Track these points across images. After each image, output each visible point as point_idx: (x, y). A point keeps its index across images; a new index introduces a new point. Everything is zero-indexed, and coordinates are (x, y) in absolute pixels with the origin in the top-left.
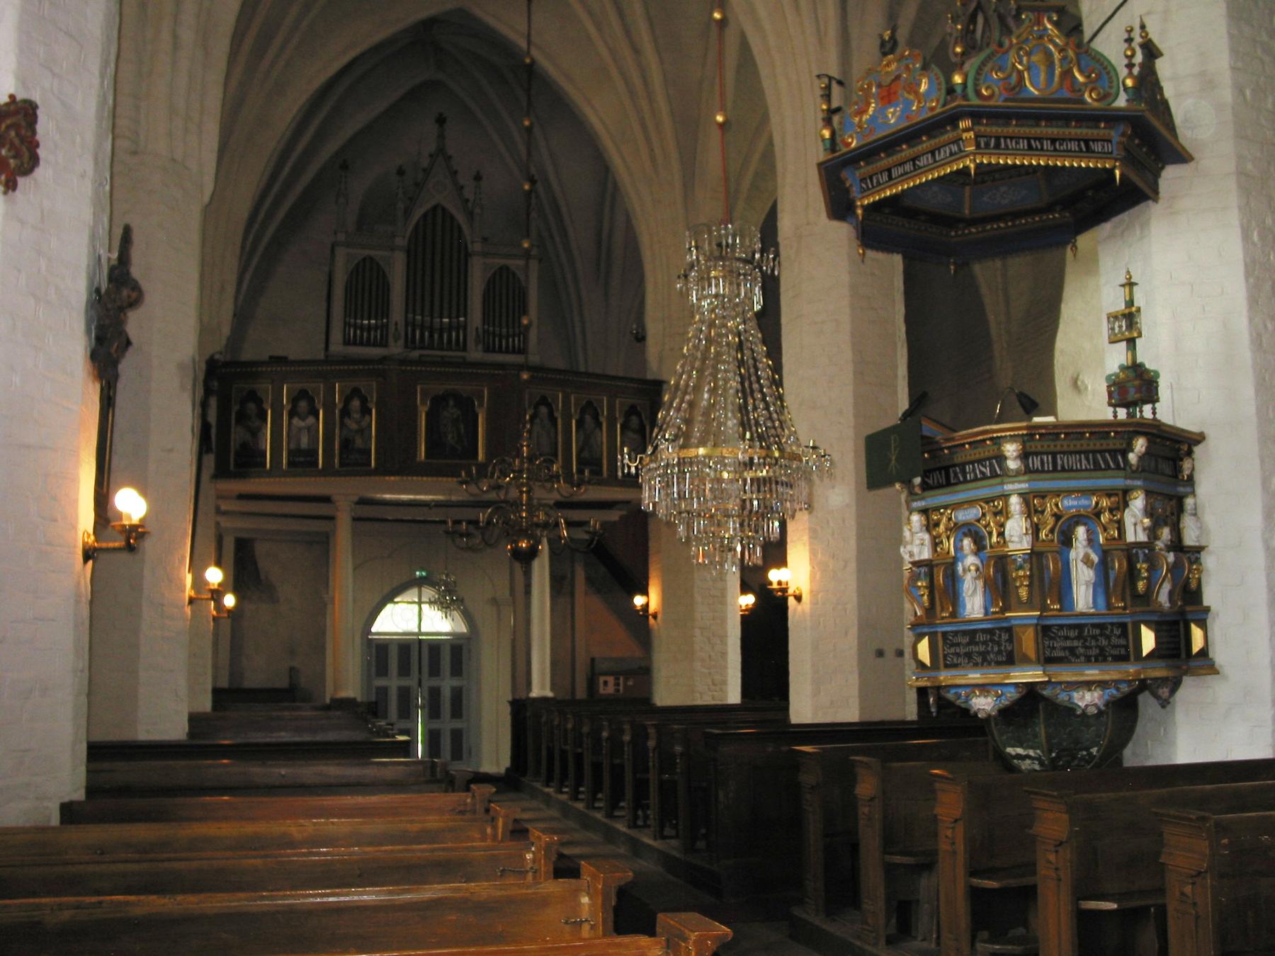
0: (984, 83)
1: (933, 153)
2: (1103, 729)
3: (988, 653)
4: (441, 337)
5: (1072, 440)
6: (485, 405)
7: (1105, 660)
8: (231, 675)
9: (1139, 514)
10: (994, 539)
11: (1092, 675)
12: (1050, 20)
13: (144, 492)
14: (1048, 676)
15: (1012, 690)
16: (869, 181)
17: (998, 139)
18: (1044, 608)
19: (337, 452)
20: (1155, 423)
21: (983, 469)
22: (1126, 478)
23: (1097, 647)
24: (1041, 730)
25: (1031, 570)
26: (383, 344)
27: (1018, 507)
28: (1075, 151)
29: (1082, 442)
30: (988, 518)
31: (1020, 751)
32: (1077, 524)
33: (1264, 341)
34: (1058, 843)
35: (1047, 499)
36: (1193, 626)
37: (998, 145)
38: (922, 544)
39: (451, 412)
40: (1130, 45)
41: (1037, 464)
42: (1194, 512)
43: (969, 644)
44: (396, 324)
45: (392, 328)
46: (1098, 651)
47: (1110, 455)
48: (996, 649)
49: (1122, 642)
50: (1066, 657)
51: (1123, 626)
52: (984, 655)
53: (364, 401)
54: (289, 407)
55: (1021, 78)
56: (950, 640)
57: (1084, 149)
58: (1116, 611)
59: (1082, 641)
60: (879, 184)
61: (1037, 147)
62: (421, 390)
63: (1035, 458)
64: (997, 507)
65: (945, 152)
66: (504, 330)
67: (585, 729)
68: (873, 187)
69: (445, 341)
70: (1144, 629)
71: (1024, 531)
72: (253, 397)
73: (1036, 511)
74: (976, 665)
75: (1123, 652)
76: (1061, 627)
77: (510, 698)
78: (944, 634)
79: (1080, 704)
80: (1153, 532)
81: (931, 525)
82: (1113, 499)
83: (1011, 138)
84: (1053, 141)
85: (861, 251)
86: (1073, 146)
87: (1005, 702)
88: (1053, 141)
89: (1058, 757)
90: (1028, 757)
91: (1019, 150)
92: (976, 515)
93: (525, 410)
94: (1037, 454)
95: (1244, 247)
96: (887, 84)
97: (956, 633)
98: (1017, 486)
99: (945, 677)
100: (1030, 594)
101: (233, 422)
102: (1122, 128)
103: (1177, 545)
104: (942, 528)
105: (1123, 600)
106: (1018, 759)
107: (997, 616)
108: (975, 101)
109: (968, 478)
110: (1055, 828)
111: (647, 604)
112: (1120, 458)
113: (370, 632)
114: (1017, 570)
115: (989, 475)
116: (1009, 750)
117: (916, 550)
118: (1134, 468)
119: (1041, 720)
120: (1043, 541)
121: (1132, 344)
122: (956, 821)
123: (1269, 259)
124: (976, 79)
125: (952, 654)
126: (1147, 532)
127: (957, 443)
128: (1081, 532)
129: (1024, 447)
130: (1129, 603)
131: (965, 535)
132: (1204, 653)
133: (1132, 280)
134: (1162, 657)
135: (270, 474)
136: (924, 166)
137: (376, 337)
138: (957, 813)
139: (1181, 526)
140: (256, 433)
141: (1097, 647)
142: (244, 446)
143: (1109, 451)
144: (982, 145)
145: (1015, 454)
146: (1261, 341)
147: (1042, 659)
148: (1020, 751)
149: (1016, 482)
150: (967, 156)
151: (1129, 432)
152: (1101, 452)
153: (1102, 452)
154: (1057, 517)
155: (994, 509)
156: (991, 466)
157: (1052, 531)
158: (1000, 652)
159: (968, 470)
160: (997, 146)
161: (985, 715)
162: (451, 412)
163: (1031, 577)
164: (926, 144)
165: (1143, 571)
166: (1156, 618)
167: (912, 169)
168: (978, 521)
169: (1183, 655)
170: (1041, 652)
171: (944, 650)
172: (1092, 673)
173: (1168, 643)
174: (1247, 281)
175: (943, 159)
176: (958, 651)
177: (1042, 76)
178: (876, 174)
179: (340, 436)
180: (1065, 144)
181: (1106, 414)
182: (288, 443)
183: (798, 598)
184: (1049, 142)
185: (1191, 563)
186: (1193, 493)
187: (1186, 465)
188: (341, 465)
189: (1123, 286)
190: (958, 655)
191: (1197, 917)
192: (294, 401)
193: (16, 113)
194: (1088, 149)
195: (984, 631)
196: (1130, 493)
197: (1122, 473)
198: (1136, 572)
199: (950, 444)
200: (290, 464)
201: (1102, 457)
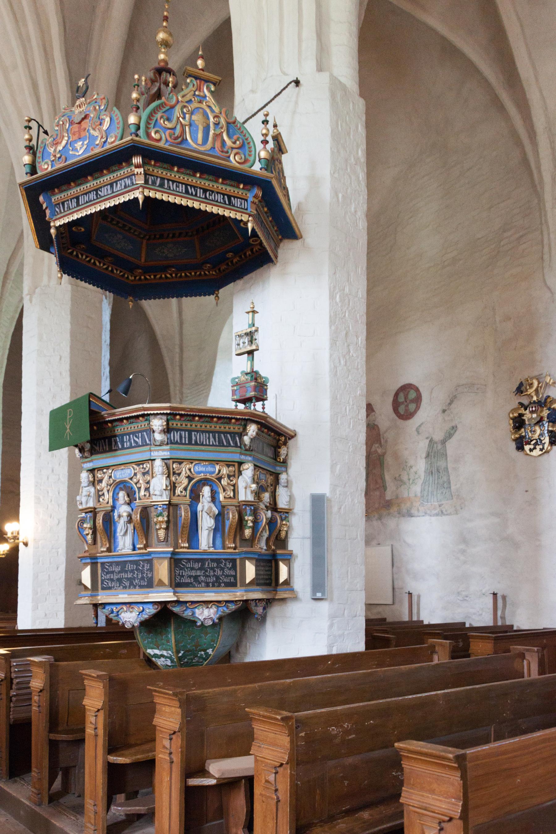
0: (154, 128)
1: (111, 185)
2: (216, 636)
5: (203, 422)
7: (219, 586)
9: (249, 481)
10: (142, 493)
11: (123, 598)
12: (208, 88)
14: (177, 596)
16: (61, 205)
18: (176, 546)
20: (263, 414)
21: (137, 440)
22: (241, 454)
24: (172, 636)
25: (168, 516)
27: (161, 469)
28: (220, 203)
29: (211, 424)
30: (138, 477)
31: (157, 652)
32: (204, 485)
34: (172, 732)
35: (183, 465)
38: (89, 496)
40: (265, 146)
41: (177, 437)
42: (286, 484)
47: (231, 436)
48: (140, 576)
50: (191, 583)
52: (131, 580)
55: (183, 132)
56: (107, 569)
57: (227, 203)
59: (203, 571)
60: (69, 208)
61: (192, 193)
63: (175, 433)
64: (145, 469)
65: (121, 185)
68: (64, 211)
70: (247, 563)
71: (164, 487)
73: (174, 473)
74: (125, 587)
75: (232, 580)
76: (189, 560)
78: (103, 564)
79: (200, 618)
80: (258, 494)
81: (96, 482)
82: (230, 468)
83: (173, 182)
84: (205, 191)
85: (59, 275)
86: (219, 198)
87: (145, 616)
88: (205, 191)
89: (184, 656)
90: (162, 656)
92: (130, 474)
94: (177, 430)
96: (77, 122)
97: (111, 563)
98: (161, 453)
99: (103, 597)
100: (167, 535)
103: (273, 507)
104: (104, 484)
105: (234, 542)
106: (155, 658)
107: (141, 551)
108: (143, 139)
109: (125, 446)
110: (171, 720)
112: (237, 439)
114: (158, 516)
115: (140, 444)
116: (149, 651)
117: (84, 500)
118: (247, 447)
119: (172, 629)
120: (179, 496)
121: (251, 356)
122: (98, 710)
123: (345, 316)
124: (148, 123)
125: (108, 579)
126: (254, 494)
127: (116, 418)
128: (206, 491)
129: (168, 424)
130: (238, 545)
131: (121, 489)
132: (287, 582)
133: (255, 309)
136: (105, 196)
138: (99, 704)
139: (277, 494)
143: (230, 433)
144: (150, 182)
145: (161, 428)
146: (336, 371)
147: (174, 584)
148: (157, 652)
149: (160, 450)
150: (138, 188)
151: (245, 419)
153: (225, 433)
154: (190, 479)
155: (142, 470)
156: (143, 437)
157: (185, 489)
158: (142, 578)
159: (125, 440)
160: (162, 185)
161: (130, 626)
163: (168, 522)
165: (249, 522)
166: (257, 557)
167: (95, 198)
168: (131, 479)
169: (273, 584)
170: (173, 579)
171: (102, 576)
172: (210, 596)
173: (263, 575)
174: (330, 327)
175: (118, 191)
176: (112, 577)
177: (200, 136)
178: (68, 200)
180: (213, 194)
181: (230, 405)
183: (26, 544)
184: (202, 191)
185: (282, 520)
186: (286, 471)
187: (283, 451)
189: (248, 313)
190: (112, 580)
191: (278, 801)
194: (230, 203)
195: (131, 562)
196: (243, 465)
197: (238, 450)
198: (245, 522)
199: (112, 418)
201: (225, 436)
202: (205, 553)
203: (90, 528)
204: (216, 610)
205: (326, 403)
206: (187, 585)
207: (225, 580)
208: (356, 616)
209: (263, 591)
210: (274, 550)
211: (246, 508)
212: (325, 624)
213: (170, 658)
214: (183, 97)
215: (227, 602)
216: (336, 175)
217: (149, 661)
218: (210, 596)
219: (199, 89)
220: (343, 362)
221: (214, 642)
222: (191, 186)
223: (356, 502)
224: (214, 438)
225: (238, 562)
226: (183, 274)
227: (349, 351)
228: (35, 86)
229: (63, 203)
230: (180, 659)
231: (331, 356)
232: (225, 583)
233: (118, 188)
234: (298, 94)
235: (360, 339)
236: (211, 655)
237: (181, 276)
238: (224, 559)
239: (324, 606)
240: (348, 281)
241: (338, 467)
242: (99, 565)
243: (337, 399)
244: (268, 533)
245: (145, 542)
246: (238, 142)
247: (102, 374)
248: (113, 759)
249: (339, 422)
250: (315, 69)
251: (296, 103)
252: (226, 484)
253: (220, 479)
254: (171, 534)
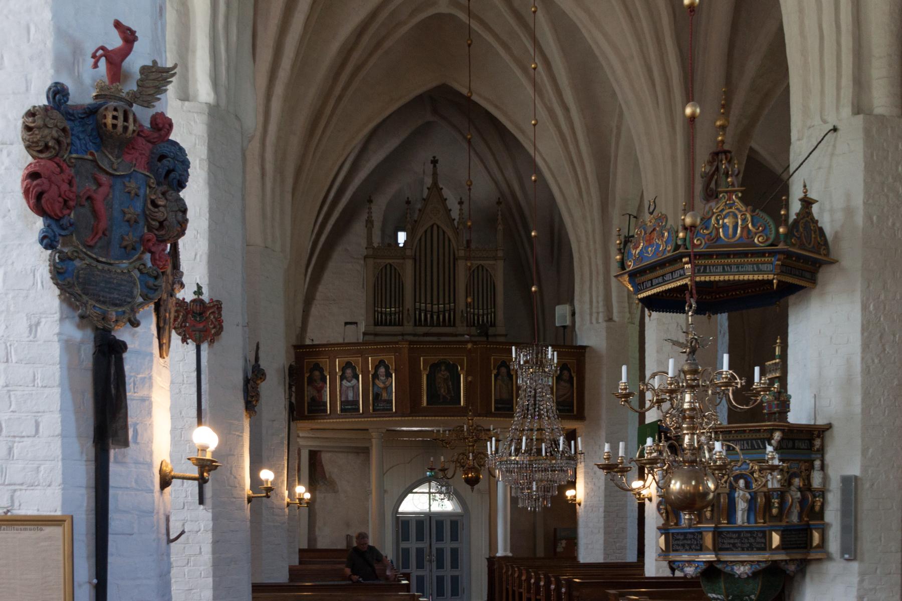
0: (696, 237)
1: (672, 273)
3: (692, 544)
4: (438, 317)
6: (465, 369)
7: (752, 550)
8: (310, 540)
13: (270, 468)
15: (702, 564)
17: (705, 267)
19: (371, 401)
23: (748, 543)
26: (401, 324)
31: (714, 596)
33: (871, 369)
36: (814, 531)
37: (705, 270)
39: (443, 374)
43: (683, 540)
44: (408, 310)
45: (406, 312)
46: (748, 545)
47: (761, 442)
48: (695, 543)
49: (763, 541)
51: (764, 532)
52: (690, 545)
53: (387, 368)
54: (340, 374)
58: (759, 525)
60: (647, 288)
62: (423, 359)
66: (481, 311)
67: (524, 578)
69: (441, 320)
70: (774, 534)
72: (317, 367)
74: (686, 550)
75: (763, 546)
76: (728, 532)
77: (488, 557)
78: (673, 534)
91: (718, 272)
93: (491, 371)
95: (862, 314)
97: (678, 533)
101: (306, 384)
102: (778, 256)
111: (575, 496)
113: (397, 512)
116: (710, 595)
130: (767, 520)
134: (784, 549)
135: (329, 417)
137: (395, 319)
140: (320, 390)
141: (748, 543)
142: (313, 399)
143: (760, 439)
147: (717, 549)
148: (714, 596)
150: (687, 277)
152: (755, 439)
158: (697, 544)
160: (705, 271)
162: (443, 374)
164: (668, 269)
174: (862, 334)
179: (373, 391)
182: (341, 397)
188: (374, 410)
190: (678, 545)
192: (343, 370)
193: (214, 306)
198: (772, 504)
200: (342, 410)
202: (740, 527)
203: (664, 509)
204: (749, 567)
205: (858, 399)
206: (727, 549)
207: (757, 546)
208: (890, 574)
209: (787, 554)
210: (807, 521)
211: (773, 493)
212: (855, 580)
214: (717, 209)
215: (758, 562)
216: (871, 201)
218: (744, 558)
219: (730, 199)
220: (876, 361)
222: (727, 265)
223: (892, 477)
224: (748, 444)
225: (767, 533)
226: (750, 291)
227: (885, 350)
228: (649, 71)
229: (643, 283)
231: (863, 359)
232: (756, 547)
233: (676, 275)
234: (836, 138)
235: (897, 336)
237: (748, 292)
238: (757, 531)
239: (855, 565)
240: (884, 288)
241: (871, 450)
242: (671, 534)
243: (869, 393)
244: (798, 509)
246: (761, 228)
247: (719, 333)
249: (872, 413)
250: (851, 114)
251: (834, 146)
252: (757, 476)
253: (752, 473)
254: (715, 515)
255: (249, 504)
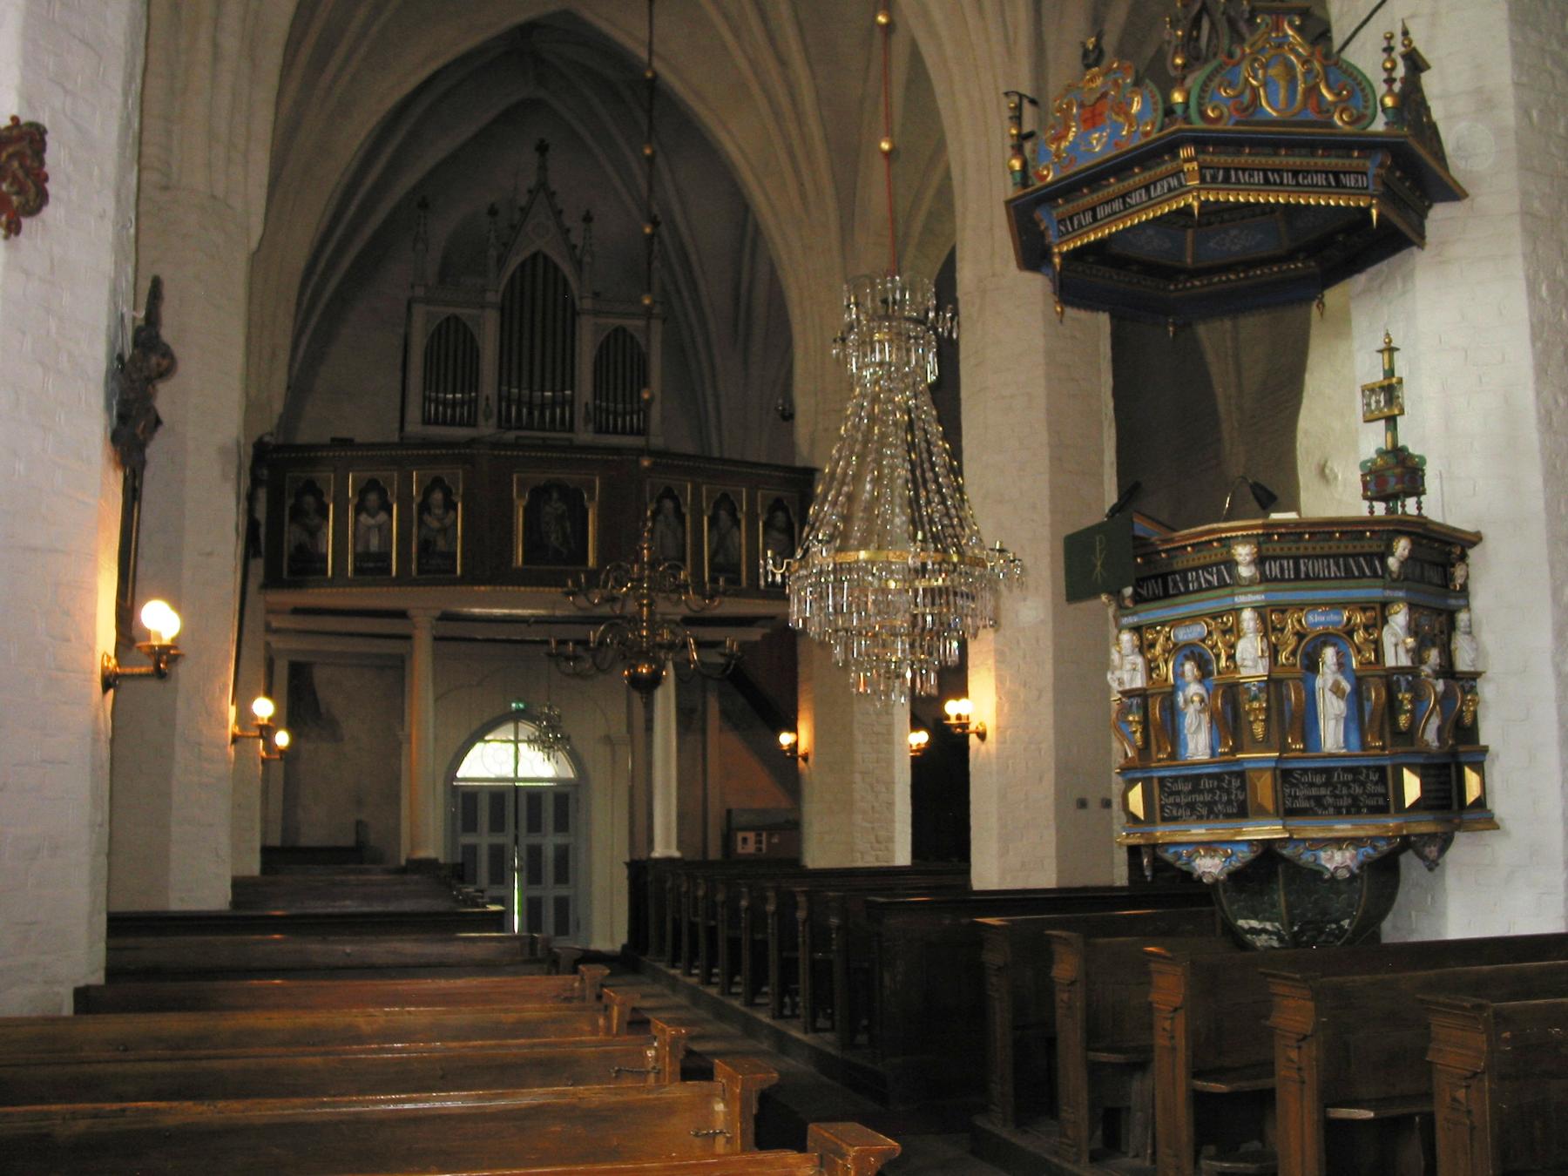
0: (1210, 102)
1: (1147, 188)
2: (1357, 897)
3: (1215, 803)
4: (542, 414)
5: (1319, 541)
6: (597, 499)
7: (1359, 812)
8: (285, 830)
9: (1401, 632)
10: (1223, 663)
13: (177, 605)
14: (1289, 831)
15: (1245, 848)
16: (1068, 223)
17: (1227, 170)
18: (1284, 748)
19: (414, 556)
20: (1420, 520)
21: (1209, 577)
22: (1385, 588)
23: (1349, 795)
24: (1281, 898)
25: (1268, 701)
26: (472, 423)
27: (1252, 624)
28: (1322, 186)
29: (1331, 543)
30: (1215, 637)
31: (1254, 924)
32: (1325, 644)
33: (1555, 419)
34: (1301, 1037)
35: (1288, 614)
36: (1467, 771)
37: (1227, 178)
38: (1134, 669)
39: (555, 506)
40: (1390, 55)
41: (1276, 570)
42: (1468, 630)
43: (1191, 792)
44: (487, 399)
45: (482, 404)
46: (1350, 801)
47: (1365, 560)
48: (1225, 798)
49: (1380, 789)
50: (1311, 809)
51: (1381, 770)
52: (1210, 806)
53: (448, 493)
54: (356, 501)
55: (1256, 96)
56: (1169, 788)
57: (1333, 184)
58: (1372, 752)
59: (1330, 789)
60: (1081, 226)
61: (1275, 180)
62: (518, 479)
63: (1273, 563)
64: (1226, 624)
65: (1163, 187)
66: (620, 406)
67: (720, 897)
68: (1074, 230)
69: (547, 419)
70: (1406, 773)
71: (1260, 654)
72: (312, 488)
73: (1274, 629)
74: (1200, 818)
75: (1381, 802)
76: (1305, 771)
77: (627, 859)
78: (1162, 780)
79: (1328, 866)
80: (1418, 654)
81: (1145, 646)
82: (1368, 614)
83: (1244, 170)
84: (1295, 173)
86: (1320, 179)
87: (1236, 864)
88: (1295, 173)
89: (1301, 932)
90: (1264, 931)
91: (1254, 184)
92: (1200, 633)
93: (646, 505)
94: (1275, 558)
95: (1530, 303)
96: (1091, 103)
97: (1175, 779)
98: (1251, 598)
99: (1162, 832)
100: (1267, 730)
101: (287, 519)
102: (1379, 157)
103: (1447, 670)
104: (1158, 649)
105: (1381, 738)
106: (1252, 934)
107: (1226, 757)
108: (1199, 124)
109: (1191, 588)
110: (1298, 1018)
111: (796, 743)
112: (1377, 563)
113: (454, 778)
114: (1251, 701)
115: (1216, 584)
116: (1241, 922)
117: (1126, 677)
118: (1395, 576)
119: (1281, 886)
120: (1283, 665)
121: (1392, 424)
122: (1176, 1010)
123: (1561, 318)
124: (1201, 97)
125: (1171, 804)
126: (1411, 654)
127: (1176, 545)
128: (1329, 654)
129: (1259, 550)
130: (1388, 742)
131: (1187, 658)
132: (1480, 803)
133: (1392, 345)
134: (1429, 808)
135: (332, 583)
136: (1137, 205)
137: (462, 414)
138: (1178, 1000)
139: (1453, 647)
140: (315, 533)
141: (1349, 795)
142: (300, 548)
143: (1364, 555)
144: (1208, 178)
145: (1248, 558)
146: (1551, 419)
147: (1281, 810)
148: (1254, 924)
149: (1250, 593)
150: (1189, 192)
151: (1389, 531)
152: (1354, 556)
153: (1355, 556)
154: (1300, 636)
155: (1222, 627)
156: (1219, 573)
157: (1294, 653)
158: (1229, 802)
159: (1190, 578)
160: (1227, 180)
161: (1211, 880)
162: (555, 506)
163: (1268, 710)
164: (1139, 177)
165: (1405, 702)
166: (1421, 761)
167: (1122, 207)
168: (1203, 640)
169: (1455, 806)
170: (1280, 802)
171: (1161, 800)
172: (1343, 828)
173: (1437, 791)
174: (1533, 345)
175: (1159, 196)
176: (1178, 800)
177: (1282, 94)
178: (1078, 214)
179: (418, 537)
180: (1310, 177)
181: (1360, 509)
182: (355, 545)
184: (1290, 175)
185: (1465, 693)
186: (1467, 607)
187: (1459, 572)
188: (420, 571)
189: (1381, 351)
190: (1178, 805)
192: (362, 493)
193: (20, 138)
194: (1339, 184)
195: (1210, 776)
196: (1390, 606)
197: (1379, 582)
198: (1397, 704)
199: (1169, 547)
200: (357, 570)
201: (1355, 562)
213: (1277, 934)
217: (1238, 940)
221: (1352, 906)
230: (1295, 935)
236: (1347, 930)
245: (1169, 749)
248: (1201, 1084)
255: (111, 692)
